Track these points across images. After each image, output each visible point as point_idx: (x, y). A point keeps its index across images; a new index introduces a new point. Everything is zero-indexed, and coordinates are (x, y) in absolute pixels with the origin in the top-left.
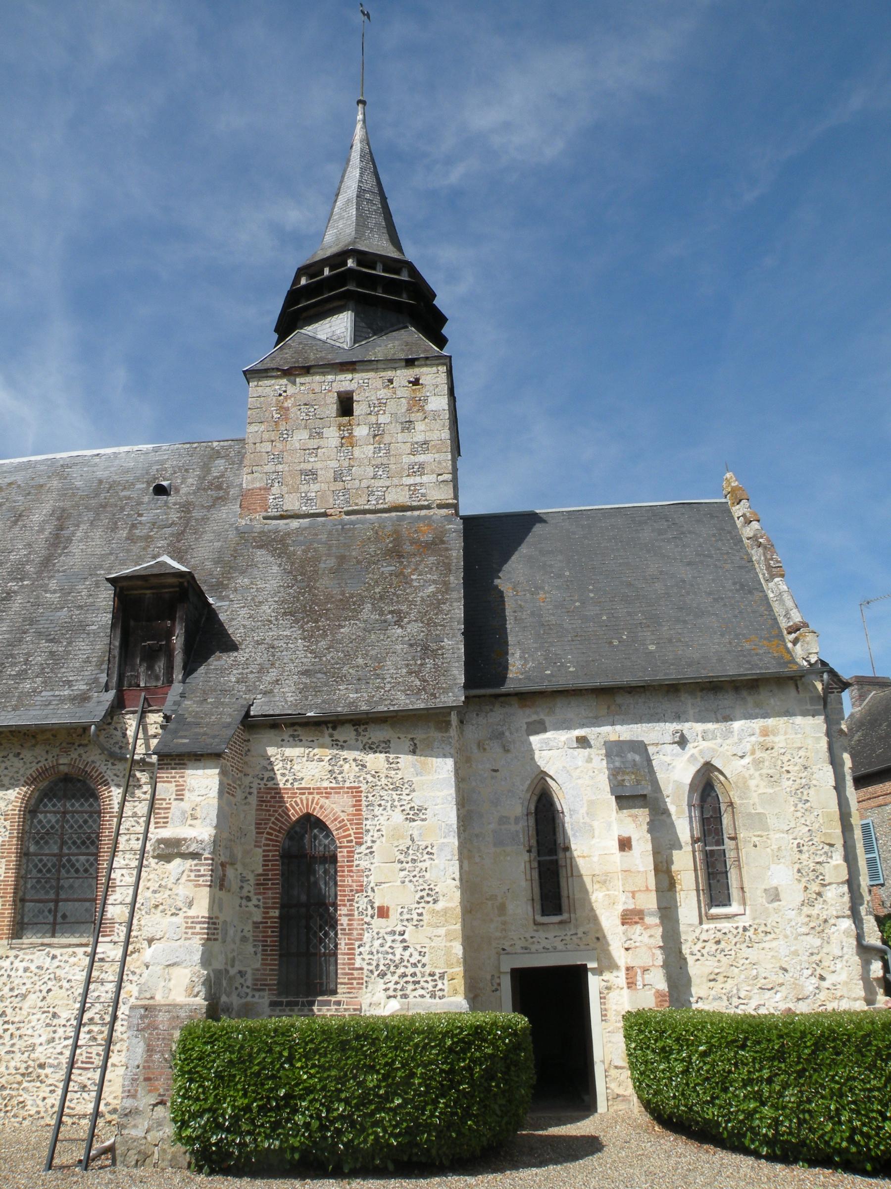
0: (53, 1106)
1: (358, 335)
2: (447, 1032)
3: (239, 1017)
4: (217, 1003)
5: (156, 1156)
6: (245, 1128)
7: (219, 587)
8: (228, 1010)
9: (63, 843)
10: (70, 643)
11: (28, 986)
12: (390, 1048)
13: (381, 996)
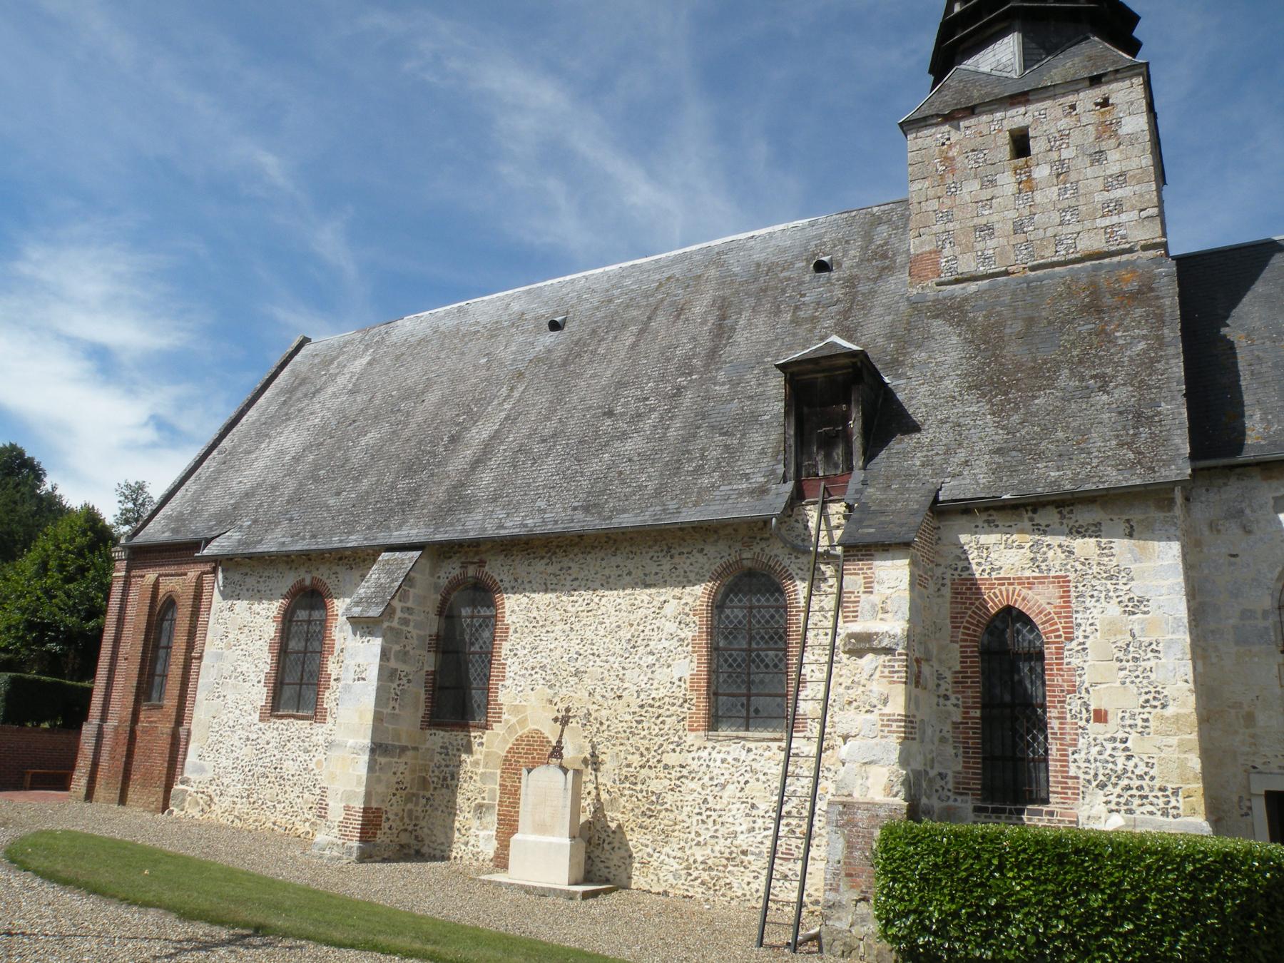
0: (757, 891)
1: (1028, 59)
2: (1189, 856)
3: (941, 820)
4: (917, 805)
5: (862, 950)
6: (953, 933)
7: (895, 364)
8: (929, 812)
9: (752, 638)
10: (744, 435)
11: (727, 776)
12: (1117, 866)
13: (1101, 809)
